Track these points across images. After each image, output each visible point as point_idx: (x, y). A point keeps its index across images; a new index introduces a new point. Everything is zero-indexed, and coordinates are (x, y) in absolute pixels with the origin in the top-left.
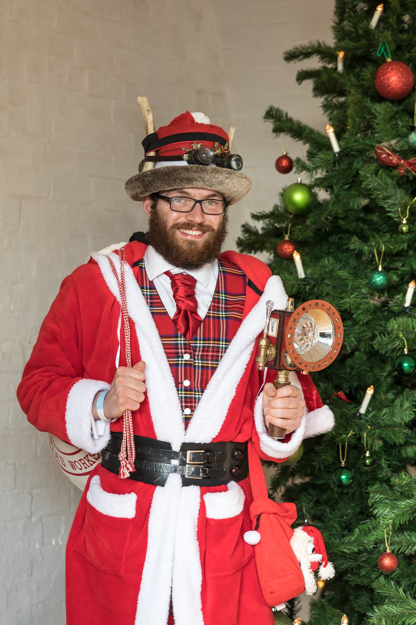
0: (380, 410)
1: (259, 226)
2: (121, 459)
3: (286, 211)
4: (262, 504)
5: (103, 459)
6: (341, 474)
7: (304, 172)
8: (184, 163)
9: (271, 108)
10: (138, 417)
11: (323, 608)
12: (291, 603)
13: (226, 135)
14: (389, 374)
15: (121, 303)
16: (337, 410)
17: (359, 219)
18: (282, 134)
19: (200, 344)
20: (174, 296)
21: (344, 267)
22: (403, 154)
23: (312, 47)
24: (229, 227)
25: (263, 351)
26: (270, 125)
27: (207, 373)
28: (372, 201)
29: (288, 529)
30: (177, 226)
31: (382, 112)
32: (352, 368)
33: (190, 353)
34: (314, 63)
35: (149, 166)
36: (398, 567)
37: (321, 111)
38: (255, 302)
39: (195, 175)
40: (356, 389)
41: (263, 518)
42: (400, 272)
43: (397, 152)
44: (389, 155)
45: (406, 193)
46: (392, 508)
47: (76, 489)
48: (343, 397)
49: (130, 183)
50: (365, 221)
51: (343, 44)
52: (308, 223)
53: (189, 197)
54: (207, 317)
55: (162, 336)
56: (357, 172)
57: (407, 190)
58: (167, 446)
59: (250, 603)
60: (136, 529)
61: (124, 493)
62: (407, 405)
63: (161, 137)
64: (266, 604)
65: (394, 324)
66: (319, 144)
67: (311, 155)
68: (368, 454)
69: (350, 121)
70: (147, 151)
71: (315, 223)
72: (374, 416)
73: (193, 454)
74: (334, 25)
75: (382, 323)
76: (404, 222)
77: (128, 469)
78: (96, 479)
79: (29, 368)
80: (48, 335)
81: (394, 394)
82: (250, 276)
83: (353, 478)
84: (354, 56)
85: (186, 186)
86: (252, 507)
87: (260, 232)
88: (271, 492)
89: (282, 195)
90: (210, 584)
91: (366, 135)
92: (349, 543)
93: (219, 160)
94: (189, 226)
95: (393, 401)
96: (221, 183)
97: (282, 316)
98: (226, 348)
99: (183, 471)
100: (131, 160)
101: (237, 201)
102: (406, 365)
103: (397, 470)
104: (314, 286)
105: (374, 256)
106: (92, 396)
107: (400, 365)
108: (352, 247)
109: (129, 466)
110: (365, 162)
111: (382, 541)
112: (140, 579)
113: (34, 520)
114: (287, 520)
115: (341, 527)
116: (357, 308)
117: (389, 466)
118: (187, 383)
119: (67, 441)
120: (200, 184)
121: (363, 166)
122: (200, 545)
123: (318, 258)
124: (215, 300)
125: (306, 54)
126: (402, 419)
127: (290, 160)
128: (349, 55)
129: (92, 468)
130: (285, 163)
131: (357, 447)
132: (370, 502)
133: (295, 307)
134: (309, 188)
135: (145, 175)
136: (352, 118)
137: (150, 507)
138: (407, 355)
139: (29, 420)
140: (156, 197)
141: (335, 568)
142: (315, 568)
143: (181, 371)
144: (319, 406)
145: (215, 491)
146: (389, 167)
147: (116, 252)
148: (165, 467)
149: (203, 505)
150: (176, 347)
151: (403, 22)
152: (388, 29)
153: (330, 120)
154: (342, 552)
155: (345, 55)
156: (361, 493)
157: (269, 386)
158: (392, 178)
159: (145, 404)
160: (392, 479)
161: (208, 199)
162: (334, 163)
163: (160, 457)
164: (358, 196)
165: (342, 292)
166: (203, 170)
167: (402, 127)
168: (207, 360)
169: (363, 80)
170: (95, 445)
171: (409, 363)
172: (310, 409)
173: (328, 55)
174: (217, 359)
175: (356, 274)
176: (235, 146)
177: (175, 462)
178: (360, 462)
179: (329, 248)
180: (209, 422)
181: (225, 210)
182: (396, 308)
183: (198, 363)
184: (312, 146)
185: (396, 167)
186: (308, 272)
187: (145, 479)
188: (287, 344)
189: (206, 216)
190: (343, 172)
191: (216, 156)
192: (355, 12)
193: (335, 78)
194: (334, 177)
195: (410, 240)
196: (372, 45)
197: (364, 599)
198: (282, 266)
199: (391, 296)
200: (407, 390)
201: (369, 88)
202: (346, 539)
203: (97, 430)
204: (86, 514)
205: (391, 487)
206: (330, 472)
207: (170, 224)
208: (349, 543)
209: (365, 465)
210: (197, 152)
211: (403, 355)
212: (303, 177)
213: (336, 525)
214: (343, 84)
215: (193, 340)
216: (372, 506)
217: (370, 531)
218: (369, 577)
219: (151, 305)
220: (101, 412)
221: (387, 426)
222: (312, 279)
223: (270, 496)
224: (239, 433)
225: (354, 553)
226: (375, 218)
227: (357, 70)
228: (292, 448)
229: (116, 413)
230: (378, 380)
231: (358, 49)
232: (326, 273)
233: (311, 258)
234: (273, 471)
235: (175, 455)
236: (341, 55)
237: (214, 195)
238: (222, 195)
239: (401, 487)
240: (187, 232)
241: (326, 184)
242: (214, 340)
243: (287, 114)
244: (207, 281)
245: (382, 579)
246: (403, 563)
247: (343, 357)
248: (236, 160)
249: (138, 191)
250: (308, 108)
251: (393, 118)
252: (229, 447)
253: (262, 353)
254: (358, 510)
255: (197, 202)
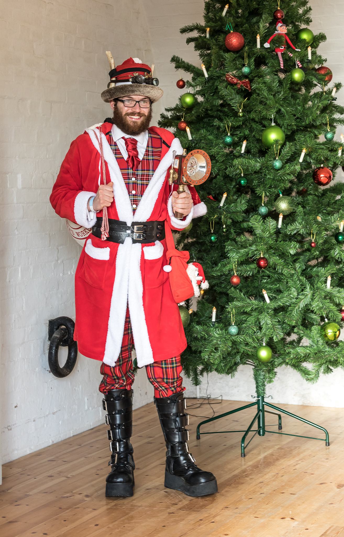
0: (230, 204)
1: (169, 114)
2: (102, 231)
3: (182, 107)
4: (172, 252)
5: (93, 231)
6: (211, 237)
7: (191, 87)
8: (130, 83)
9: (174, 56)
10: (110, 209)
11: (203, 304)
12: (188, 301)
13: (150, 69)
14: (234, 187)
15: (100, 153)
16: (208, 205)
17: (218, 110)
18: (180, 69)
19: (140, 173)
20: (127, 149)
21: (211, 134)
22: (240, 78)
23: (194, 26)
24: (153, 115)
25: (171, 175)
26: (174, 65)
27: (144, 187)
28: (224, 101)
29: (185, 264)
30: (128, 114)
31: (229, 57)
32: (216, 184)
33: (135, 177)
34: (195, 34)
35: (113, 85)
36: (240, 282)
37: (199, 57)
38: (167, 151)
39: (136, 89)
40: (218, 194)
41: (173, 258)
42: (239, 136)
43: (236, 77)
44: (232, 78)
45: (241, 97)
46: (237, 253)
47: (80, 246)
48: (212, 198)
49: (103, 94)
50: (221, 111)
51: (209, 24)
52: (193, 112)
53: (133, 100)
54: (143, 159)
55: (121, 169)
56: (217, 87)
57: (242, 96)
58: (125, 223)
59: (167, 301)
60: (111, 264)
61: (103, 248)
62: (243, 202)
63: (118, 70)
64: (175, 302)
65: (236, 162)
66: (198, 74)
67: (194, 79)
68: (224, 227)
69: (213, 62)
70: (111, 77)
71: (196, 113)
72: (227, 208)
73: (138, 227)
74: (204, 15)
75: (231, 161)
76: (241, 111)
77: (105, 236)
78: (89, 241)
79: (56, 187)
80: (65, 170)
81: (237, 196)
82: (164, 138)
83: (217, 238)
84: (214, 30)
85: (131, 94)
86: (167, 253)
87: (170, 117)
88: (177, 246)
89: (180, 99)
90: (147, 292)
91: (221, 69)
92: (216, 271)
93: (147, 81)
94: (133, 114)
95: (236, 200)
96: (149, 92)
97: (181, 158)
98: (153, 174)
99: (133, 236)
100: (103, 82)
101: (156, 101)
102: (242, 182)
103: (239, 234)
104: (197, 144)
105: (226, 128)
106: (87, 200)
107: (240, 182)
108: (215, 124)
109: (106, 234)
110: (221, 82)
111: (232, 270)
112: (112, 290)
113: (59, 262)
114: (185, 260)
115: (212, 263)
116: (218, 154)
117: (235, 232)
118: (134, 192)
119: (75, 223)
120: (138, 93)
121: (219, 84)
122: (142, 273)
123: (198, 130)
124: (147, 151)
125: (190, 29)
126: (241, 209)
127: (183, 82)
128: (212, 30)
129: (87, 236)
130: (181, 83)
131: (219, 223)
132: (226, 250)
133: (187, 154)
134: (193, 95)
135: (111, 89)
136: (214, 60)
137: (116, 254)
138: (243, 177)
139: (56, 212)
140: (116, 100)
141: (209, 283)
142: (199, 283)
143: (131, 186)
144: (199, 203)
145: (149, 246)
146: (232, 85)
147: (97, 128)
148: (123, 234)
149: (143, 252)
150: (128, 174)
151: (238, 13)
152: (231, 16)
153: (203, 62)
154: (213, 275)
155: (210, 30)
156: (221, 246)
157: (175, 193)
158: (234, 89)
159: (113, 203)
160: (237, 239)
161: (142, 100)
162: (206, 83)
163: (121, 229)
164: (218, 99)
165: (210, 147)
166: (139, 86)
167: (239, 64)
168: (144, 181)
169: (219, 42)
170: (89, 224)
171: (244, 181)
172: (195, 204)
173: (201, 30)
174: (148, 180)
175: (217, 137)
176: (154, 74)
177: (129, 232)
178: (220, 231)
179: (204, 125)
180: (145, 211)
181: (151, 106)
182: (237, 154)
183: (139, 182)
184: (194, 75)
185: (236, 84)
186: (193, 137)
187: (114, 240)
188: (184, 172)
189: (142, 109)
190: (210, 87)
191: (146, 79)
192: (215, 8)
193: (205, 41)
194: (205, 89)
195: (243, 120)
196: (224, 25)
197: (224, 299)
198: (180, 134)
199: (235, 148)
200: (243, 194)
201: (222, 45)
202: (215, 269)
203: (90, 216)
204: (85, 259)
205: (236, 242)
206: (205, 236)
207: (124, 113)
208: (216, 271)
209: (223, 232)
210: (136, 77)
211: (241, 177)
212: (191, 90)
213: (209, 262)
214: (209, 44)
215: (136, 170)
216: (227, 252)
217: (226, 265)
218: (226, 288)
219: (116, 154)
220: (91, 208)
221: (233, 212)
222: (195, 140)
223: (176, 248)
224: (160, 216)
225: (219, 276)
226: (226, 109)
227: (216, 37)
228: (186, 224)
229: (99, 208)
230: (229, 189)
231: (216, 26)
232: (202, 137)
233: (195, 130)
234: (177, 236)
235: (129, 228)
236: (208, 29)
237: (145, 98)
238: (149, 98)
239: (241, 242)
240: (133, 117)
241: (201, 93)
242: (147, 171)
243: (182, 59)
244: (143, 141)
245: (232, 289)
246: (243, 281)
247: (211, 179)
248: (156, 81)
249: (108, 97)
250: (193, 57)
251: (234, 60)
252: (155, 224)
253: (171, 176)
254: (220, 254)
255: (137, 102)
